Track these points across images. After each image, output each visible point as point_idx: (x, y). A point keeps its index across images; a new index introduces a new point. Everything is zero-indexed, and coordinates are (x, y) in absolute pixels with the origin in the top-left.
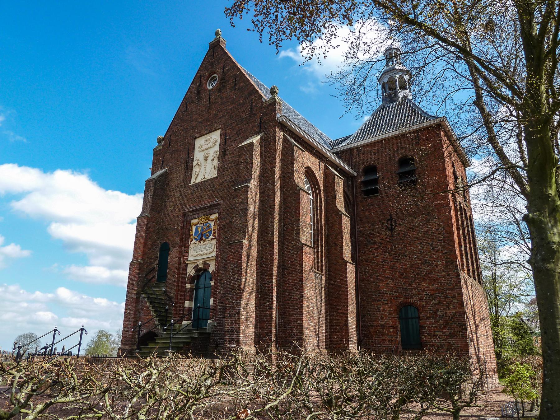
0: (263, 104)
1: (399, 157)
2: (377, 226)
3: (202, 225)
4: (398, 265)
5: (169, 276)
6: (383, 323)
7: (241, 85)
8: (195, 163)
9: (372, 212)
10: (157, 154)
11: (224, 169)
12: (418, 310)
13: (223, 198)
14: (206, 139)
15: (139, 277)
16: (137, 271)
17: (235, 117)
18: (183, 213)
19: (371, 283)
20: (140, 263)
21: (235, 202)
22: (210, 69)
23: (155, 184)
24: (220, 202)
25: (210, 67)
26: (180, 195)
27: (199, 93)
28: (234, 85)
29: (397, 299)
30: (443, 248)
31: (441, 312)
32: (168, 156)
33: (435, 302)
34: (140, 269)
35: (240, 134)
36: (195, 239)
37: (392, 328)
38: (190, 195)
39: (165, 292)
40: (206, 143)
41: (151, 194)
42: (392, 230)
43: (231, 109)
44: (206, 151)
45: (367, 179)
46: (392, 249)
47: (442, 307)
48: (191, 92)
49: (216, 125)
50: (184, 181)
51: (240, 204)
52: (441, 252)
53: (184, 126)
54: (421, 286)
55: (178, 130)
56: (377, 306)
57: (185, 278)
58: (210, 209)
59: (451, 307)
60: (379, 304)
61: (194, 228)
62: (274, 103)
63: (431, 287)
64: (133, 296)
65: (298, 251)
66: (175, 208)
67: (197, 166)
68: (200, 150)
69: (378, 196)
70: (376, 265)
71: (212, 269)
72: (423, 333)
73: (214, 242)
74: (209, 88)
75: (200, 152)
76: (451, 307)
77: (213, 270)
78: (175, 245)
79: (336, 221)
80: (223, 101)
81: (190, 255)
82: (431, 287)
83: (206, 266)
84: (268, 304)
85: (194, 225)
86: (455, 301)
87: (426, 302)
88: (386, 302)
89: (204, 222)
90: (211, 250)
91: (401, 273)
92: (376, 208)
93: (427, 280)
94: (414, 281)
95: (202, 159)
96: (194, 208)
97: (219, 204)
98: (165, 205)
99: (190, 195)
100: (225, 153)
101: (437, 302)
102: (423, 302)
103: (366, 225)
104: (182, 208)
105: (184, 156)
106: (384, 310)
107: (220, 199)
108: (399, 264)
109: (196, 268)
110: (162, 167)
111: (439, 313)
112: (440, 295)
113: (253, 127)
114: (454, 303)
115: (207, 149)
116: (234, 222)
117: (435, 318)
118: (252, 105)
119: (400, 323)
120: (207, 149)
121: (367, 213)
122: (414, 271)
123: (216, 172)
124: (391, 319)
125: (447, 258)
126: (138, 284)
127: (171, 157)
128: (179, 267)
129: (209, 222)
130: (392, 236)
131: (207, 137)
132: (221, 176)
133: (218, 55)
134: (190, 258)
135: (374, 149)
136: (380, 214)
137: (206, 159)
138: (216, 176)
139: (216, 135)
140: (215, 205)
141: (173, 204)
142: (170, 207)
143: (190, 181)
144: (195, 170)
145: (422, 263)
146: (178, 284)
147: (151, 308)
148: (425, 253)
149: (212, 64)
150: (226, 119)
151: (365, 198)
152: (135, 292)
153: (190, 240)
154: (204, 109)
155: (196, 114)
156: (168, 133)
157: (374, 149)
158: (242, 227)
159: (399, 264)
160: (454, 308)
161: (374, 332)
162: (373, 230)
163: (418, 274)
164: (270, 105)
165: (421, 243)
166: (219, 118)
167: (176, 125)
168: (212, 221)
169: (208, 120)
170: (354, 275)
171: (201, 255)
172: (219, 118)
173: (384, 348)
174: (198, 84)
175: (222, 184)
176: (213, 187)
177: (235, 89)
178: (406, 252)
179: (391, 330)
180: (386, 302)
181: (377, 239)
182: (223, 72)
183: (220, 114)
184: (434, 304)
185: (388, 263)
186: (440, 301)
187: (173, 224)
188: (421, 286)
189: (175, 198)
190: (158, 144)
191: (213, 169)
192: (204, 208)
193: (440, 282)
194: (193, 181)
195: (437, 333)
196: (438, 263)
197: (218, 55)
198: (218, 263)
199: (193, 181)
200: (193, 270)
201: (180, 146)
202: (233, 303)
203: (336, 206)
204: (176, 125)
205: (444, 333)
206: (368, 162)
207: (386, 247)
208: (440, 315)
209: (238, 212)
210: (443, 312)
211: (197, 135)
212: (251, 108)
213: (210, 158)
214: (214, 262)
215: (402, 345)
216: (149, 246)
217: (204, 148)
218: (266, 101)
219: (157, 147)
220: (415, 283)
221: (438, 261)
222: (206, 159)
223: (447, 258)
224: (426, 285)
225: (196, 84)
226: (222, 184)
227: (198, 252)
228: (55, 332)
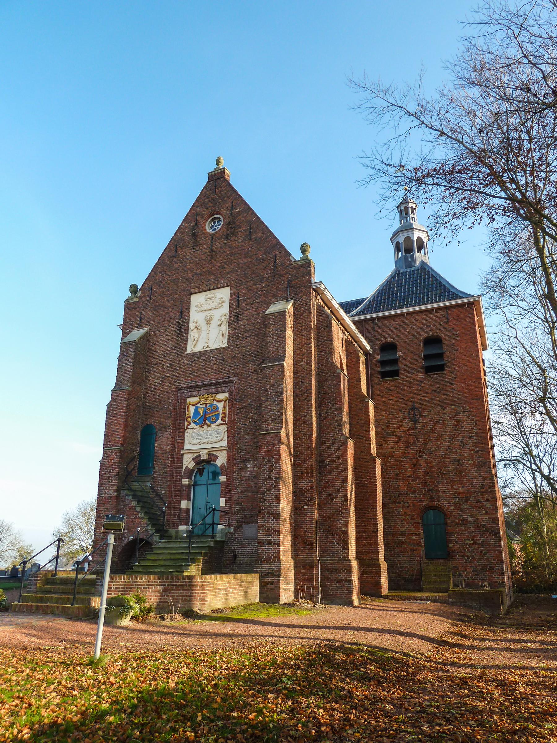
0: (292, 264)
1: (425, 335)
2: (397, 416)
3: (204, 406)
4: (421, 462)
5: (157, 468)
6: (404, 529)
7: (259, 235)
8: (192, 326)
9: (391, 398)
10: (129, 306)
11: (237, 338)
12: (445, 515)
13: (237, 374)
14: (208, 297)
15: (120, 468)
16: (117, 460)
17: (251, 275)
18: (177, 388)
20: (121, 451)
21: (266, 383)
22: (210, 207)
23: (136, 347)
24: (234, 379)
25: (211, 204)
26: (170, 365)
27: (194, 235)
28: (247, 233)
29: (421, 501)
30: (475, 445)
31: (472, 518)
32: (149, 312)
33: (465, 507)
34: (121, 457)
35: (259, 296)
36: (194, 422)
37: (414, 536)
38: (186, 367)
39: (152, 488)
40: (208, 302)
41: (131, 359)
42: (415, 421)
43: (245, 263)
45: (385, 359)
46: (415, 443)
47: (473, 513)
48: (182, 233)
49: (222, 281)
50: (177, 347)
51: (273, 385)
52: (472, 450)
53: (173, 275)
54: (449, 487)
55: (163, 280)
56: (396, 509)
58: (218, 386)
59: (484, 512)
61: (192, 409)
64: (111, 493)
65: (341, 446)
66: (163, 381)
67: (196, 330)
68: (199, 310)
69: (398, 379)
70: (395, 461)
72: (451, 542)
73: (224, 428)
75: (199, 312)
76: (484, 512)
77: (223, 463)
78: (165, 429)
79: (361, 409)
80: (233, 251)
84: (306, 507)
85: (192, 405)
86: (488, 505)
87: (454, 506)
88: (407, 505)
89: (208, 401)
90: (220, 438)
91: (425, 472)
92: (395, 394)
93: (456, 481)
94: (441, 481)
95: (202, 323)
96: (193, 384)
97: (232, 382)
98: (147, 377)
99: (186, 367)
100: (238, 319)
101: (467, 506)
102: (451, 506)
103: (383, 413)
104: (175, 382)
105: (174, 314)
106: (405, 514)
107: (233, 375)
108: (424, 461)
109: (198, 461)
110: (140, 326)
111: (470, 519)
112: (471, 499)
113: (277, 290)
114: (487, 508)
116: (264, 407)
117: (464, 524)
118: (275, 262)
119: (423, 530)
121: (384, 399)
122: (441, 470)
123: (226, 341)
124: (413, 525)
125: (479, 457)
126: (119, 478)
127: (153, 314)
128: (172, 457)
129: (215, 403)
130: (416, 428)
131: (209, 294)
132: (233, 346)
133: (222, 191)
134: (187, 447)
135: (394, 323)
136: (401, 402)
137: (208, 322)
138: (226, 345)
139: (224, 294)
140: (225, 383)
141: (159, 375)
142: (155, 379)
143: (186, 348)
144: (193, 334)
145: (451, 461)
146: (171, 479)
147: (138, 509)
148: (454, 450)
149: (214, 201)
150: (238, 275)
151: (383, 381)
152: (115, 488)
153: (186, 424)
154: (204, 257)
156: (147, 282)
157: (394, 323)
159: (424, 461)
160: (487, 513)
161: (393, 539)
162: (392, 419)
163: (446, 474)
164: (302, 266)
165: (450, 438)
166: (228, 273)
167: (161, 272)
168: (220, 401)
169: (210, 273)
170: (380, 472)
171: (204, 443)
172: (228, 273)
173: (405, 559)
174: (192, 224)
175: (235, 357)
176: (223, 360)
178: (431, 448)
179: (414, 538)
180: (407, 505)
181: (396, 430)
183: (229, 268)
184: (465, 509)
186: (471, 506)
187: (161, 401)
188: (449, 487)
189: (163, 368)
190: (130, 295)
191: (221, 337)
192: (210, 385)
193: (472, 484)
194: (190, 349)
195: (467, 542)
196: (470, 462)
197: (222, 191)
198: (230, 457)
199: (190, 349)
200: (193, 462)
202: (269, 507)
204: (161, 272)
205: (475, 541)
206: (386, 338)
207: (407, 441)
209: (270, 396)
210: (474, 517)
211: (194, 290)
212: (275, 265)
213: (214, 323)
214: (225, 453)
215: (426, 555)
216: (130, 428)
217: (205, 307)
218: (296, 261)
219: (129, 299)
220: (443, 483)
221: (469, 460)
223: (479, 457)
224: (455, 487)
225: (190, 222)
226: (235, 357)
227: (200, 439)
228: (59, 541)
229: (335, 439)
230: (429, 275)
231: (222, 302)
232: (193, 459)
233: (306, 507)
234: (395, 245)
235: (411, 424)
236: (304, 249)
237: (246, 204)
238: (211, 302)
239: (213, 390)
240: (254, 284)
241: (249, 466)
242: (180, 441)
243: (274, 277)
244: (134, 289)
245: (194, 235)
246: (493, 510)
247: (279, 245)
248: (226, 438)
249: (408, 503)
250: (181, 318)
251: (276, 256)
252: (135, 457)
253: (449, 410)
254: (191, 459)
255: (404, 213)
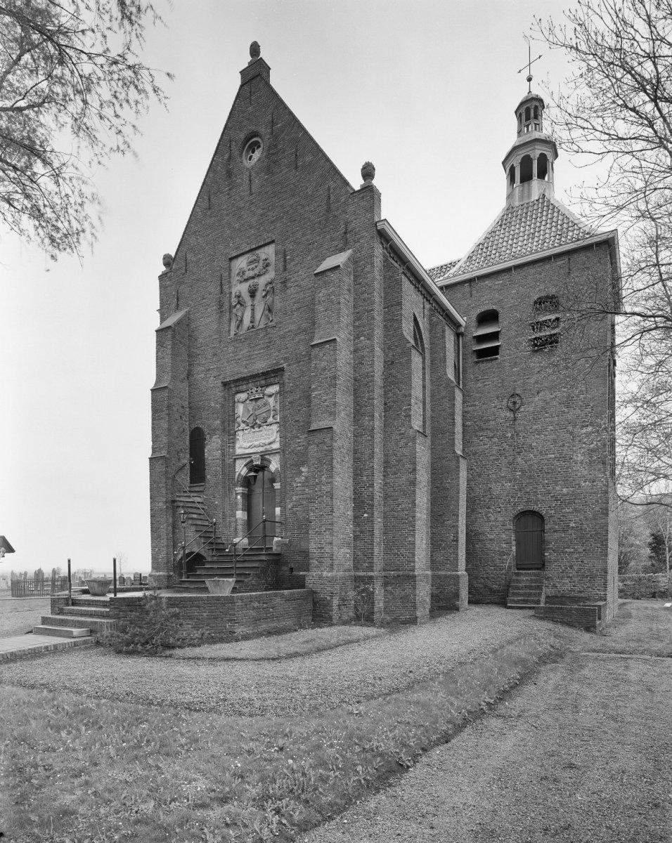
4: (519, 459)
19: (479, 484)
27: (229, 174)
31: (575, 523)
33: (568, 511)
36: (244, 422)
40: (251, 267)
44: (251, 282)
46: (512, 437)
57: (233, 479)
60: (489, 512)
62: (369, 194)
63: (565, 490)
64: (161, 504)
69: (497, 359)
71: (274, 465)
74: (248, 164)
75: (241, 282)
78: (213, 432)
81: (237, 445)
82: (565, 490)
83: (265, 462)
84: (366, 515)
90: (271, 440)
95: (246, 296)
100: (285, 286)
106: (496, 520)
110: (178, 308)
111: (572, 525)
115: (253, 278)
120: (253, 278)
121: (479, 385)
153: (236, 425)
155: (227, 215)
158: (328, 406)
168: (270, 396)
174: (226, 157)
177: (296, 167)
179: (504, 546)
182: (272, 133)
185: (506, 457)
200: (245, 469)
201: (206, 270)
203: (446, 374)
208: (573, 527)
222: (253, 293)
227: (251, 441)
229: (402, 434)
230: (548, 206)
231: (267, 266)
232: (245, 465)
233: (366, 515)
234: (508, 171)
235: (510, 415)
236: (368, 172)
237: (291, 113)
238: (253, 266)
239: (263, 382)
240: (304, 235)
241: (303, 470)
242: (231, 445)
243: (327, 220)
244: (168, 261)
245: (229, 174)
246: (602, 513)
247: (333, 171)
248: (278, 439)
249: (500, 507)
250: (222, 293)
251: (329, 189)
252: (185, 465)
253: (558, 394)
254: (243, 466)
255: (524, 117)
